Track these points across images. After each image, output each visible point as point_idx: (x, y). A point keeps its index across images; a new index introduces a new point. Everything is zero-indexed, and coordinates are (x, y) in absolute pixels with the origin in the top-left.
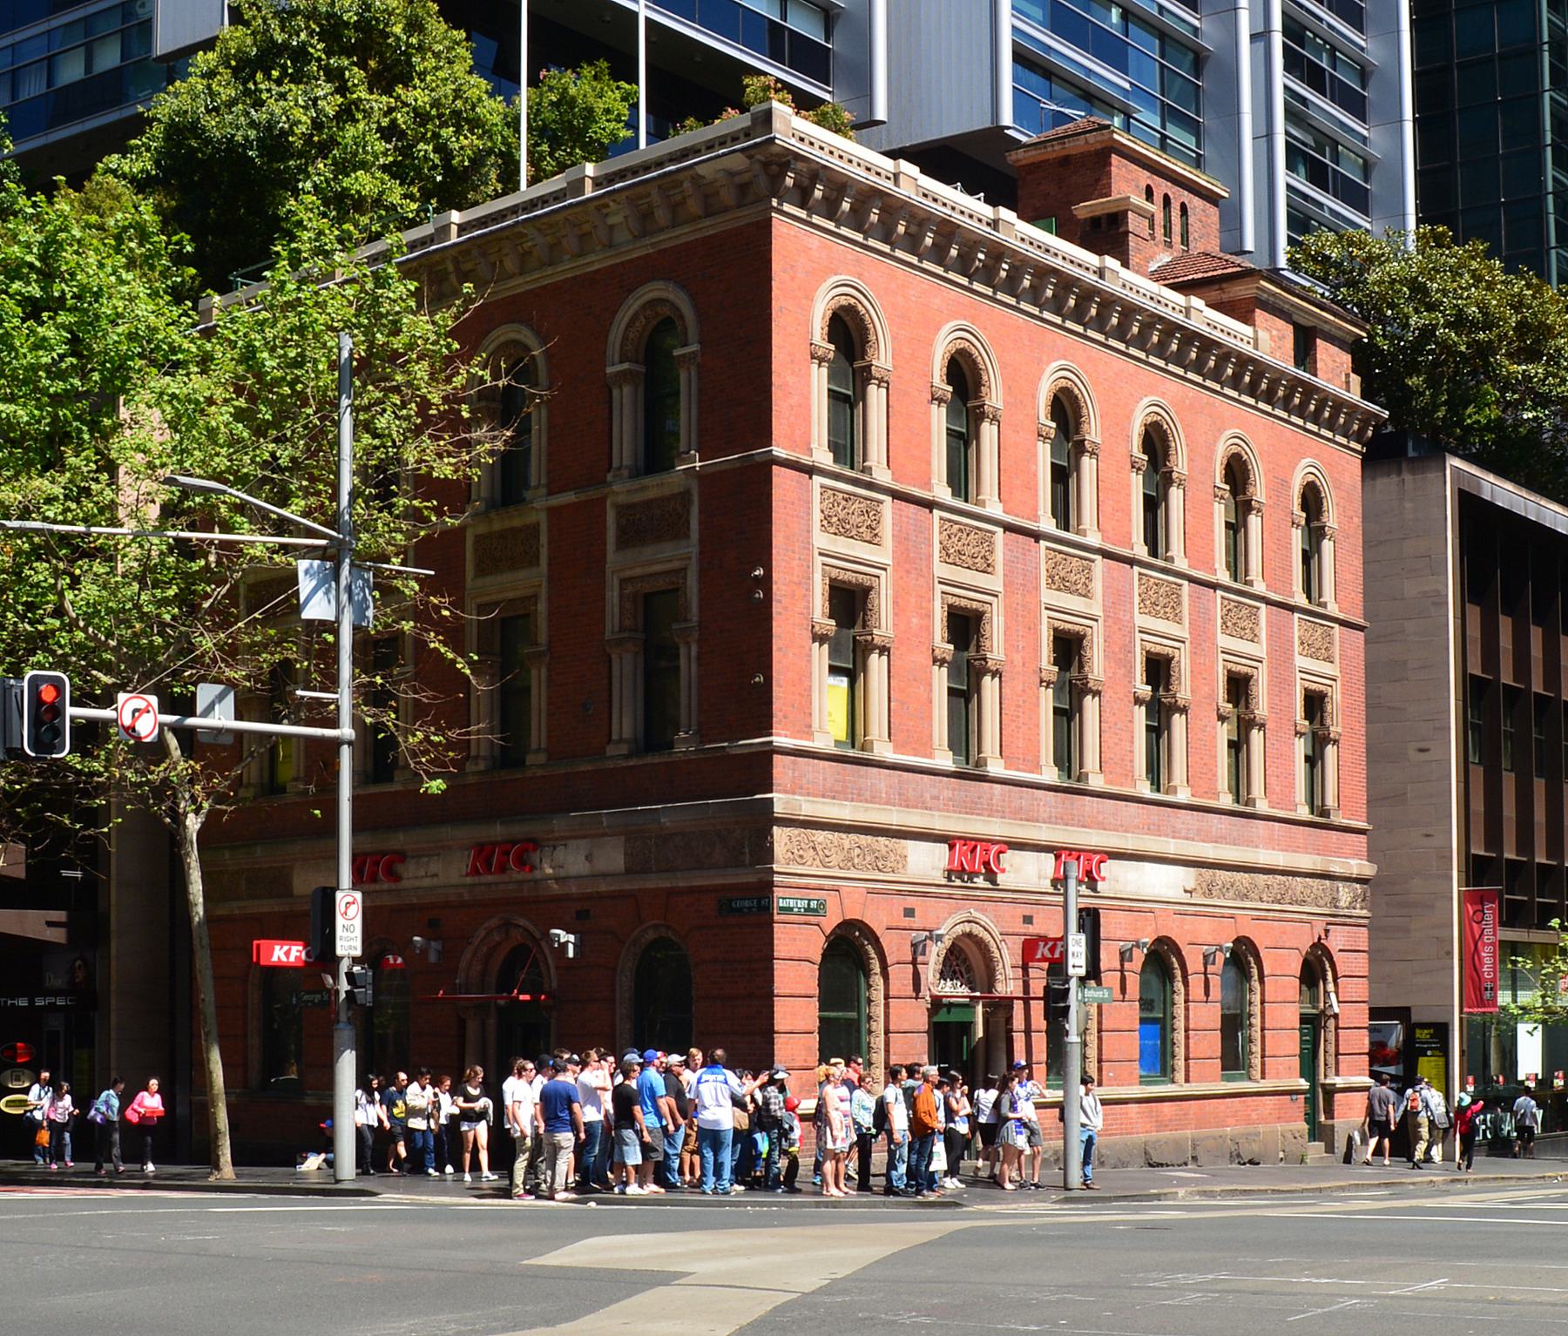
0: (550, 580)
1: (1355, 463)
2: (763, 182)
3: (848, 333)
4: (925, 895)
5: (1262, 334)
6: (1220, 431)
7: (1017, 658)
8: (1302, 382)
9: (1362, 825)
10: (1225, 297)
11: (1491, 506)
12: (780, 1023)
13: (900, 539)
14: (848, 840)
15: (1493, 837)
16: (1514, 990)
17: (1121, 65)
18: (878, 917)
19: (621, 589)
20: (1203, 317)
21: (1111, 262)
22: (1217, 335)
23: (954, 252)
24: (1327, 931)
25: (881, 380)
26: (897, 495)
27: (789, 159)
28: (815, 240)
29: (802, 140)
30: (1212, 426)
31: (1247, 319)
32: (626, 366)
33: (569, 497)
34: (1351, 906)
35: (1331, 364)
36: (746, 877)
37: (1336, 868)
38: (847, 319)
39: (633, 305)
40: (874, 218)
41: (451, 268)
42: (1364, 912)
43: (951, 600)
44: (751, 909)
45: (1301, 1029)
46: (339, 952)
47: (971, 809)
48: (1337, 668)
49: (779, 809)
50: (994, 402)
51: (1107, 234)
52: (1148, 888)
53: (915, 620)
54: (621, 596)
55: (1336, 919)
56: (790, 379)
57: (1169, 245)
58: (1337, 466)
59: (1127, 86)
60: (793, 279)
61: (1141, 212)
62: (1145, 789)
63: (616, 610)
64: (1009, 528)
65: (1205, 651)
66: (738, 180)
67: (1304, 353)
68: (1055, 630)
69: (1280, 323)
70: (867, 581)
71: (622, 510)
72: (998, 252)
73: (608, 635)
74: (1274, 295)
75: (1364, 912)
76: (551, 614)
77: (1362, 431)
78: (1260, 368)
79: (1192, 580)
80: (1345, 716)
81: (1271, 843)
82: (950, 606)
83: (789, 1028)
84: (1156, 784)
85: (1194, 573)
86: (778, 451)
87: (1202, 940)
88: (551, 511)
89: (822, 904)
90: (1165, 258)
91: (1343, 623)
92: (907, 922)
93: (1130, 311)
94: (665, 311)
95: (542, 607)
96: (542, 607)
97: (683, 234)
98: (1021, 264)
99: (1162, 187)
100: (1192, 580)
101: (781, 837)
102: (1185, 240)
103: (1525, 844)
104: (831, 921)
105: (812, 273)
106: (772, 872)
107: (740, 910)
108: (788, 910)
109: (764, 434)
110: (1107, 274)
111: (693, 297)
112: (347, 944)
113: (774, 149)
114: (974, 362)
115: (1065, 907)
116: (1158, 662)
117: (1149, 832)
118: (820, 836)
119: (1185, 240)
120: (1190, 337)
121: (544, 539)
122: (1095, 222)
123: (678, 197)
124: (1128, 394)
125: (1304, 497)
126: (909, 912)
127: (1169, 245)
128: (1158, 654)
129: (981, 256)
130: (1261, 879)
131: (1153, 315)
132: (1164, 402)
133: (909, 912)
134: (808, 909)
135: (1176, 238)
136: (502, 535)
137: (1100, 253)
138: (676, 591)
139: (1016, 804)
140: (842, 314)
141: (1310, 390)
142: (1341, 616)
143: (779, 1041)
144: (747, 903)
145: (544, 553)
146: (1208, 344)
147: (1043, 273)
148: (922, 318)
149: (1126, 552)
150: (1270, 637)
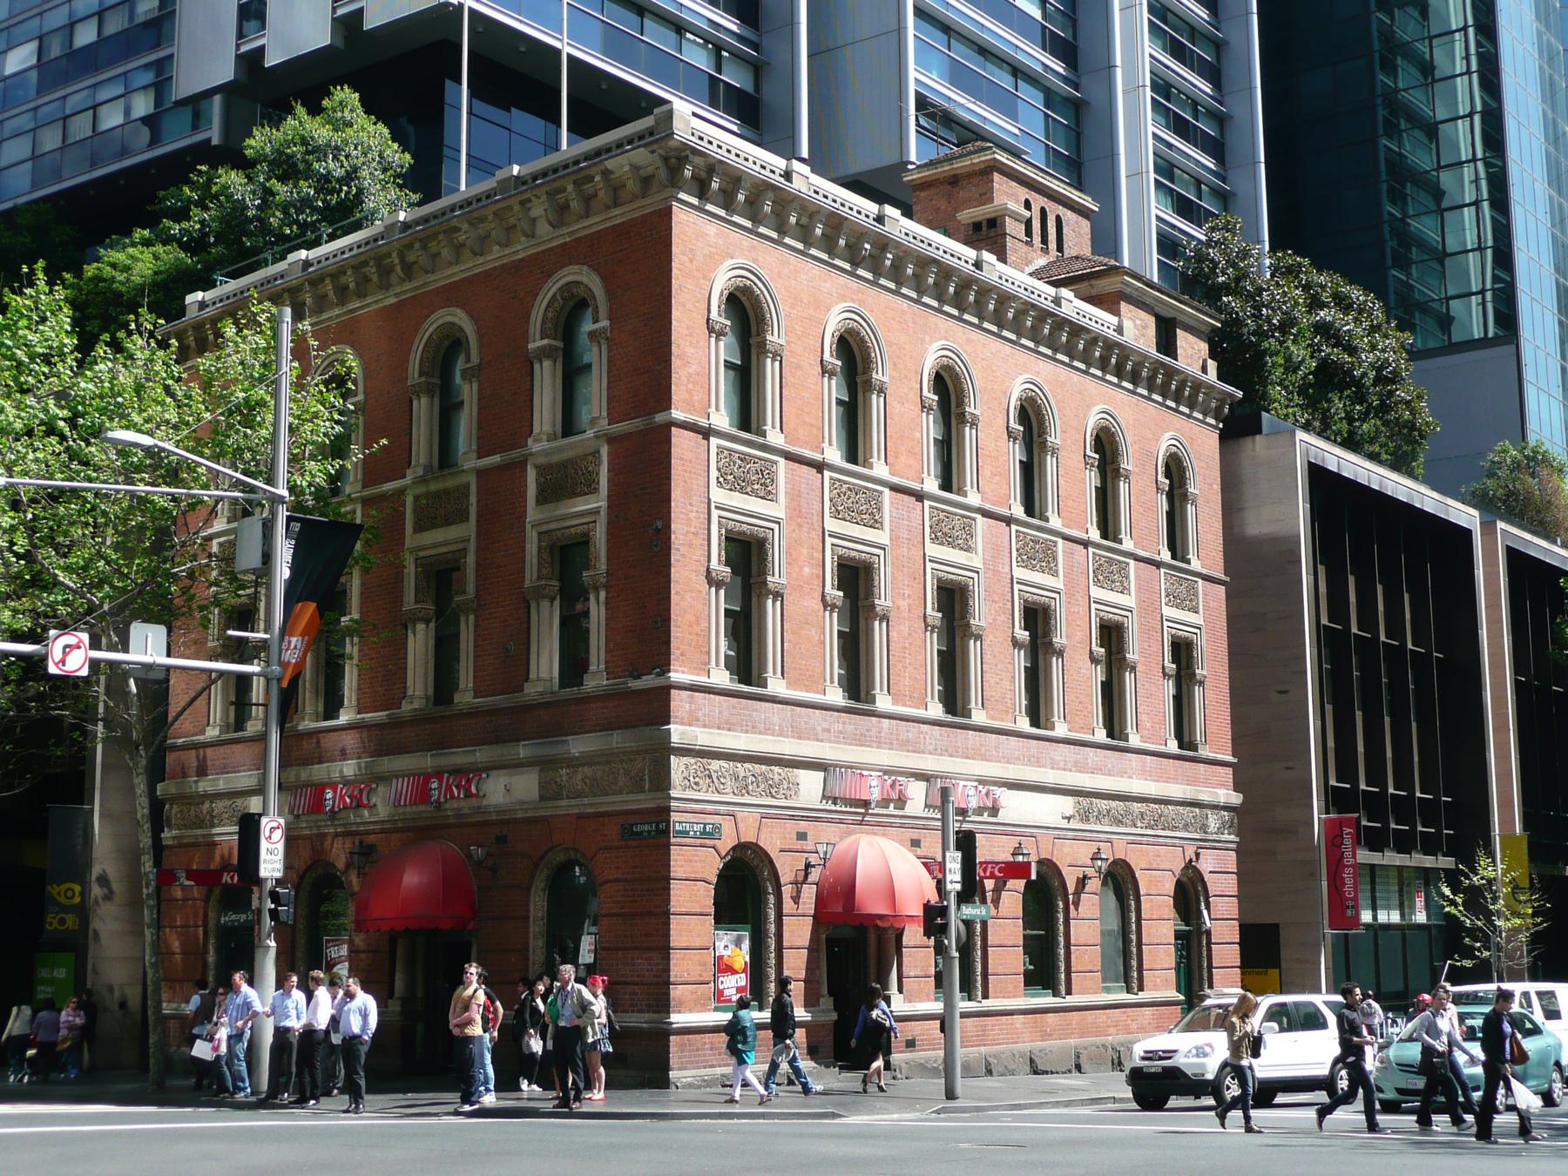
0: (478, 535)
1: (1216, 436)
2: (663, 174)
3: (745, 313)
4: (817, 819)
5: (1127, 324)
6: (1089, 407)
7: (903, 604)
8: (1163, 365)
9: (1230, 759)
10: (1094, 292)
11: (1338, 476)
12: (675, 940)
13: (794, 495)
14: (742, 769)
15: (1346, 769)
16: (1374, 910)
17: (1012, 115)
18: (773, 841)
19: (540, 541)
20: (1073, 306)
21: (988, 257)
22: (1084, 322)
23: (842, 242)
24: (1198, 855)
25: (775, 354)
26: (790, 457)
27: (685, 153)
28: (712, 229)
29: (701, 138)
30: (1082, 402)
31: (1116, 312)
32: (546, 342)
33: (496, 459)
34: (1219, 831)
35: (1190, 351)
36: (644, 801)
37: (1205, 796)
38: (743, 299)
39: (551, 289)
40: (767, 209)
41: (397, 261)
42: (1232, 837)
43: (841, 551)
44: (650, 834)
45: (1176, 945)
46: (263, 873)
47: (861, 740)
48: (1205, 618)
49: (675, 739)
50: (880, 376)
51: (988, 234)
52: (1034, 816)
53: (806, 569)
54: (540, 549)
55: (1204, 844)
56: (690, 350)
57: (1045, 251)
58: (1201, 442)
59: (1016, 131)
60: (691, 261)
61: (1016, 217)
62: (1024, 724)
63: (535, 561)
64: (895, 489)
65: (1079, 597)
66: (643, 173)
67: (1167, 344)
68: (939, 580)
69: (1142, 314)
70: (761, 533)
71: (542, 470)
72: (883, 244)
73: (527, 583)
74: (1137, 289)
75: (1232, 837)
76: (478, 565)
77: (1219, 409)
78: (1125, 352)
79: (1066, 538)
80: (1213, 665)
81: (1145, 774)
82: (840, 557)
83: (684, 945)
84: (1035, 723)
85: (1067, 531)
86: (677, 414)
87: (1073, 860)
88: (481, 473)
89: (717, 828)
90: (1041, 261)
91: (1206, 578)
92: (799, 845)
93: (1005, 298)
94: (582, 292)
95: (471, 559)
96: (471, 559)
97: (596, 223)
98: (904, 255)
99: (1038, 201)
100: (1066, 538)
101: (677, 764)
102: (1060, 248)
103: (1376, 777)
104: (727, 842)
105: (709, 254)
106: (670, 798)
107: (637, 834)
108: (685, 834)
109: (665, 402)
110: (985, 266)
111: (604, 279)
112: (270, 866)
113: (671, 143)
114: (863, 340)
115: (944, 830)
116: (1035, 610)
117: (1029, 763)
118: (715, 765)
119: (1060, 248)
120: (1061, 323)
121: (473, 499)
122: (977, 226)
123: (591, 191)
124: (1002, 372)
125: (1167, 465)
126: (802, 836)
127: (1045, 251)
128: (1034, 603)
129: (867, 246)
130: (1136, 807)
131: (1026, 303)
132: (1039, 380)
133: (802, 836)
134: (704, 832)
135: (1053, 245)
136: (438, 495)
137: (978, 249)
138: (584, 542)
139: (903, 736)
140: (738, 294)
141: (1171, 372)
142: (1204, 571)
143: (675, 956)
144: (646, 828)
145: (473, 510)
146: (1077, 330)
147: (924, 262)
148: (815, 302)
149: (1004, 511)
150: (1138, 589)
